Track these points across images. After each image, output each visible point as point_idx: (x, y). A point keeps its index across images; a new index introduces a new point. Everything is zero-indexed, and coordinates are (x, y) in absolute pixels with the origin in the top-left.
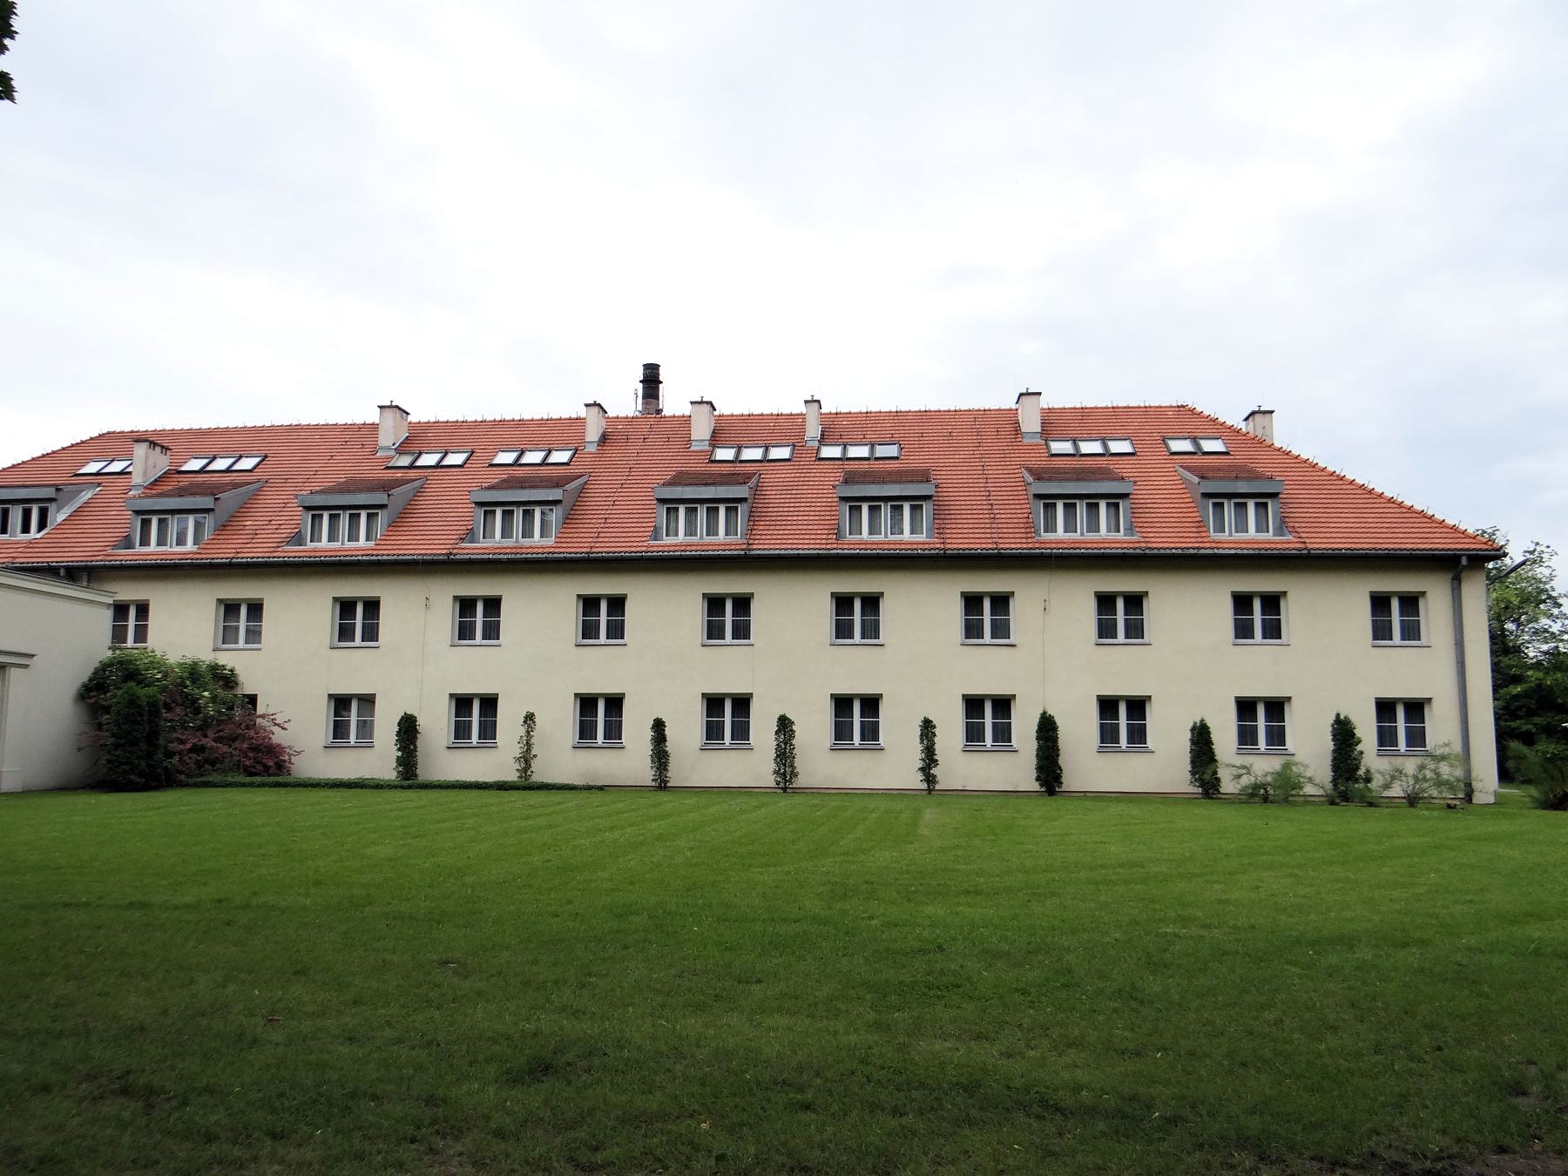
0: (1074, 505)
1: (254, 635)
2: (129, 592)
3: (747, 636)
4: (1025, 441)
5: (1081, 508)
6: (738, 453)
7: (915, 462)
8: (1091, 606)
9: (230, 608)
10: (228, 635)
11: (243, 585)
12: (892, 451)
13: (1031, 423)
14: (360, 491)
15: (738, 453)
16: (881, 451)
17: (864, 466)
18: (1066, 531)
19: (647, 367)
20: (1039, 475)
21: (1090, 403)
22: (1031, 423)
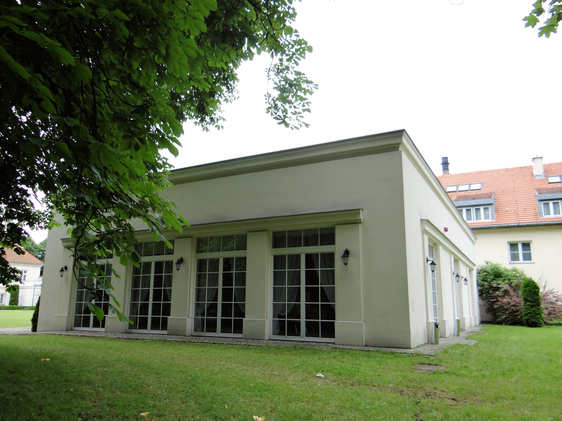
0: (470, 209)
1: (528, 257)
2: (520, 237)
3: (530, 259)
4: (537, 178)
5: (473, 210)
6: (457, 188)
7: (486, 191)
8: (507, 248)
9: (513, 246)
10: (515, 257)
11: (17, 273)
12: (478, 186)
13: (538, 171)
14: (556, 192)
15: (457, 188)
16: (473, 187)
17: (466, 193)
18: (555, 214)
19: (444, 158)
20: (540, 191)
21: (483, 169)
22: (538, 171)
